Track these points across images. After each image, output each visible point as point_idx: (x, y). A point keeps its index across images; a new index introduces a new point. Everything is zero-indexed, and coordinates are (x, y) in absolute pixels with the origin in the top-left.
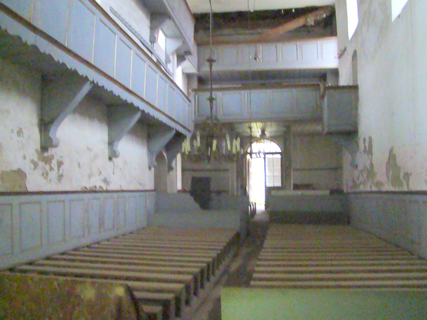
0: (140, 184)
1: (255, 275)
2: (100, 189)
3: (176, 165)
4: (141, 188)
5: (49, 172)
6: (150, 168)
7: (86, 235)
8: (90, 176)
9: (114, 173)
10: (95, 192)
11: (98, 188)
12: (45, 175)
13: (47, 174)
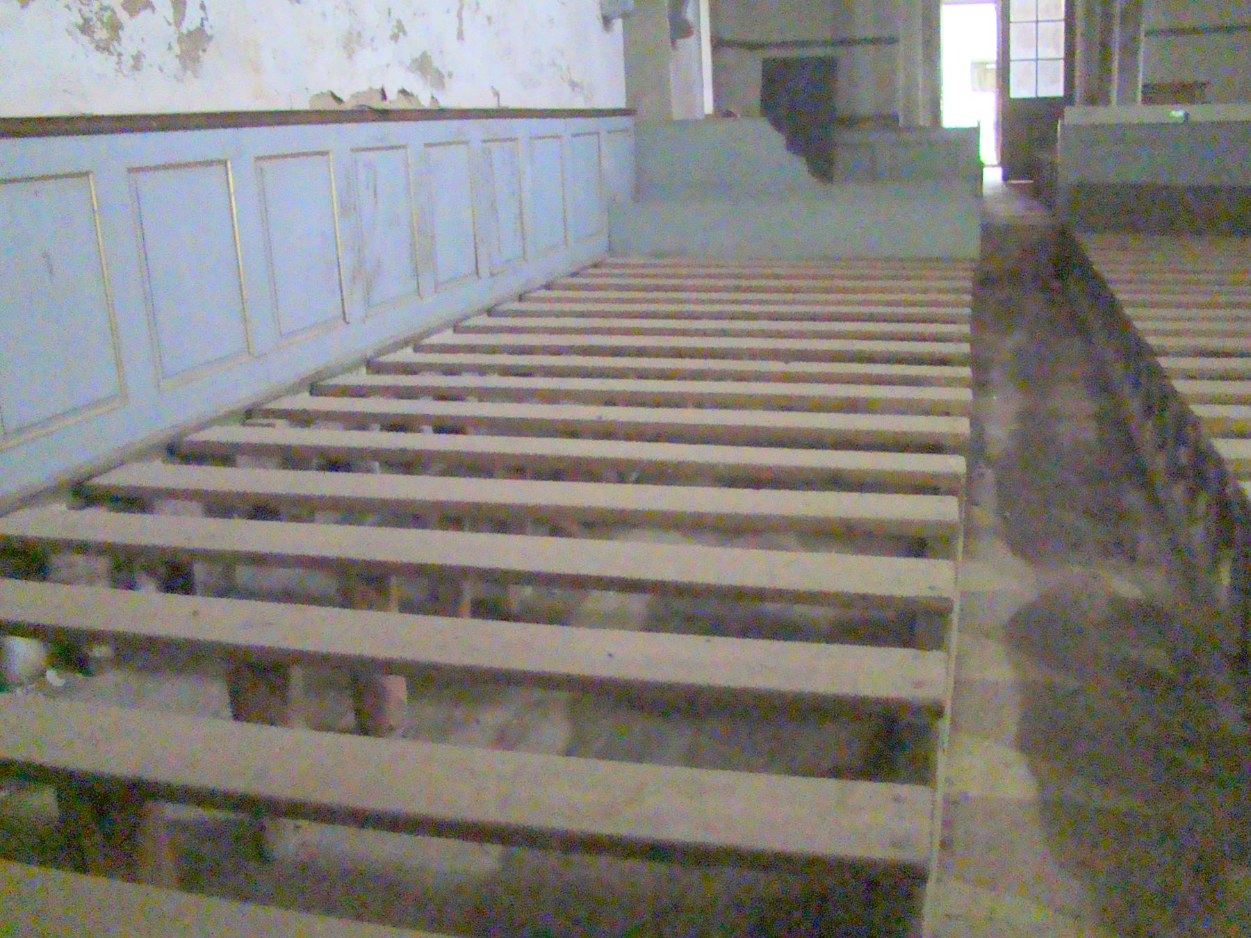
0: (573, 85)
1: (966, 372)
2: (403, 104)
3: (698, 15)
4: (579, 104)
5: (123, 16)
6: (607, 21)
7: (355, 308)
8: (352, 42)
9: (460, 36)
10: (384, 115)
11: (394, 101)
12: (102, 34)
13: (115, 27)
